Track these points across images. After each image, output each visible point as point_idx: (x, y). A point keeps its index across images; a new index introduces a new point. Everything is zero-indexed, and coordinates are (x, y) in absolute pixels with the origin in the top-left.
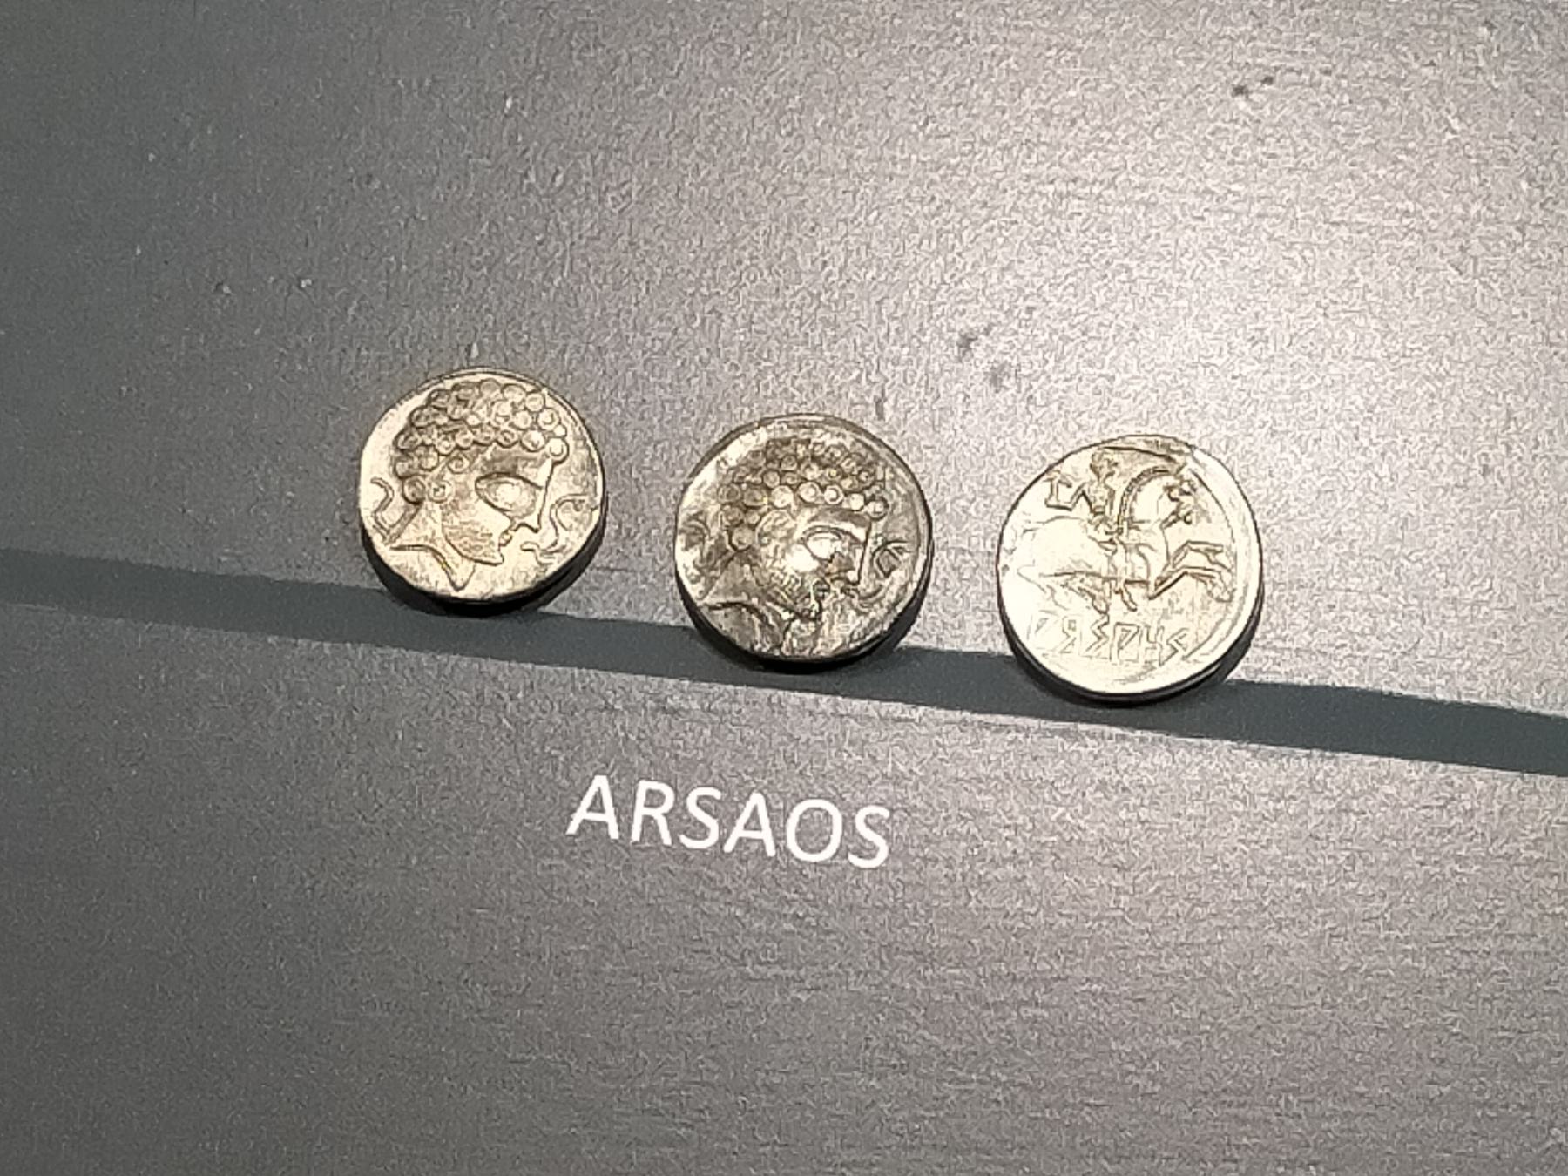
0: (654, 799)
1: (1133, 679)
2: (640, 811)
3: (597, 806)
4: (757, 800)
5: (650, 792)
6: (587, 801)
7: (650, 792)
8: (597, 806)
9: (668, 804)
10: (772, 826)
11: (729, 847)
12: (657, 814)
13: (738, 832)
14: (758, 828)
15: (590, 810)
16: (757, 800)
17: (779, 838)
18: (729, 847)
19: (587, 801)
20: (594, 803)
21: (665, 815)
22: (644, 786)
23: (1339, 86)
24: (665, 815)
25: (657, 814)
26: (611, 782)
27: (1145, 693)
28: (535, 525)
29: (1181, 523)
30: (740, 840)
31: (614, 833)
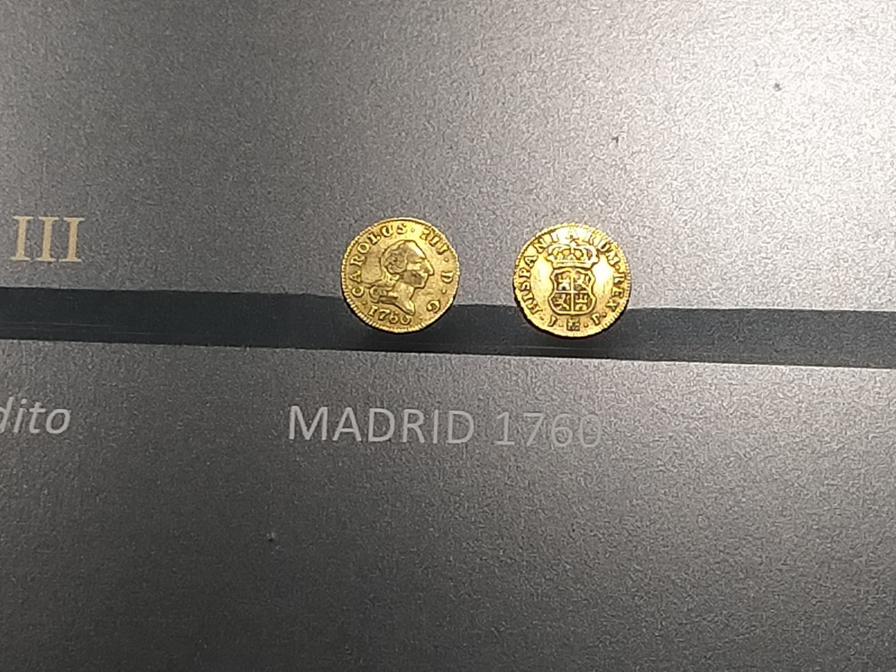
2: (406, 426)
3: (348, 424)
4: (349, 410)
6: (341, 424)
8: (348, 424)
9: (421, 422)
11: (335, 438)
12: (415, 426)
13: (340, 429)
14: (351, 427)
15: (344, 427)
18: (335, 438)
19: (341, 424)
20: (345, 423)
21: (420, 426)
23: (630, 634)
24: (420, 426)
25: (415, 426)
29: (532, 270)
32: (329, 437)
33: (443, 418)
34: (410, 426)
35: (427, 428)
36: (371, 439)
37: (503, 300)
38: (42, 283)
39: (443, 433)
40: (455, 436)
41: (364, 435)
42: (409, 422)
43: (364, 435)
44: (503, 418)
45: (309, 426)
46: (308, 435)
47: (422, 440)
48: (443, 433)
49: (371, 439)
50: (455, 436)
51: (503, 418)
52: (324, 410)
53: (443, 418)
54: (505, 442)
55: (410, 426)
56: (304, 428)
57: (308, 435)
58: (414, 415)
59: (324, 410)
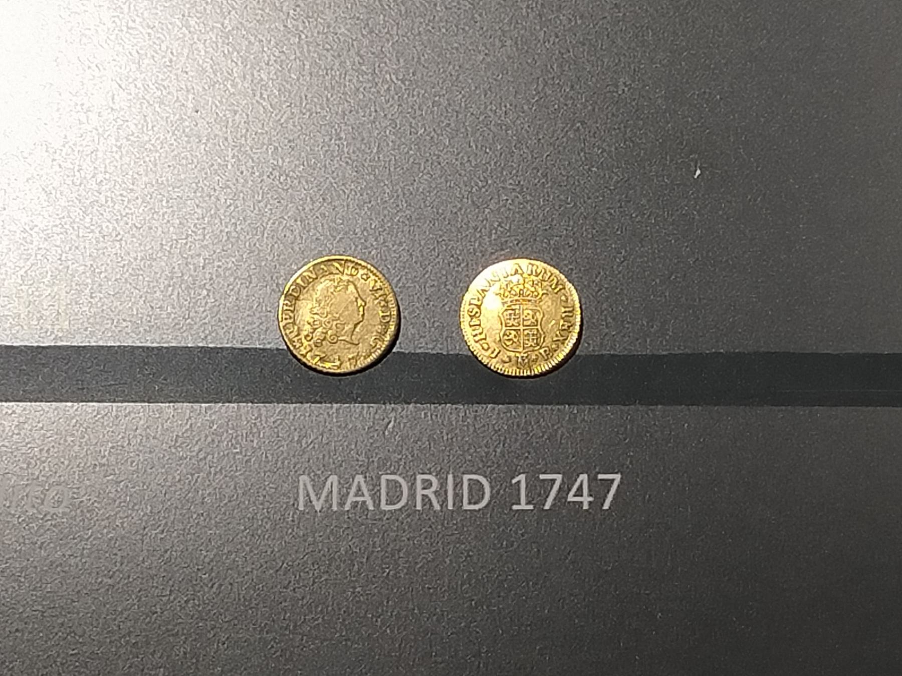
0: (427, 485)
2: (420, 492)
4: (359, 478)
7: (424, 481)
8: (579, 493)
13: (351, 499)
24: (435, 492)
32: (341, 504)
33: (458, 485)
34: (425, 492)
35: (441, 493)
36: (384, 507)
37: (272, 342)
38: (322, 360)
39: (458, 496)
40: (390, 502)
41: (377, 505)
43: (377, 505)
44: (519, 482)
47: (437, 507)
48: (458, 496)
49: (466, 507)
50: (390, 502)
51: (519, 482)
52: (333, 479)
53: (458, 485)
54: (523, 506)
55: (425, 492)
56: (313, 497)
58: (427, 480)
59: (333, 479)
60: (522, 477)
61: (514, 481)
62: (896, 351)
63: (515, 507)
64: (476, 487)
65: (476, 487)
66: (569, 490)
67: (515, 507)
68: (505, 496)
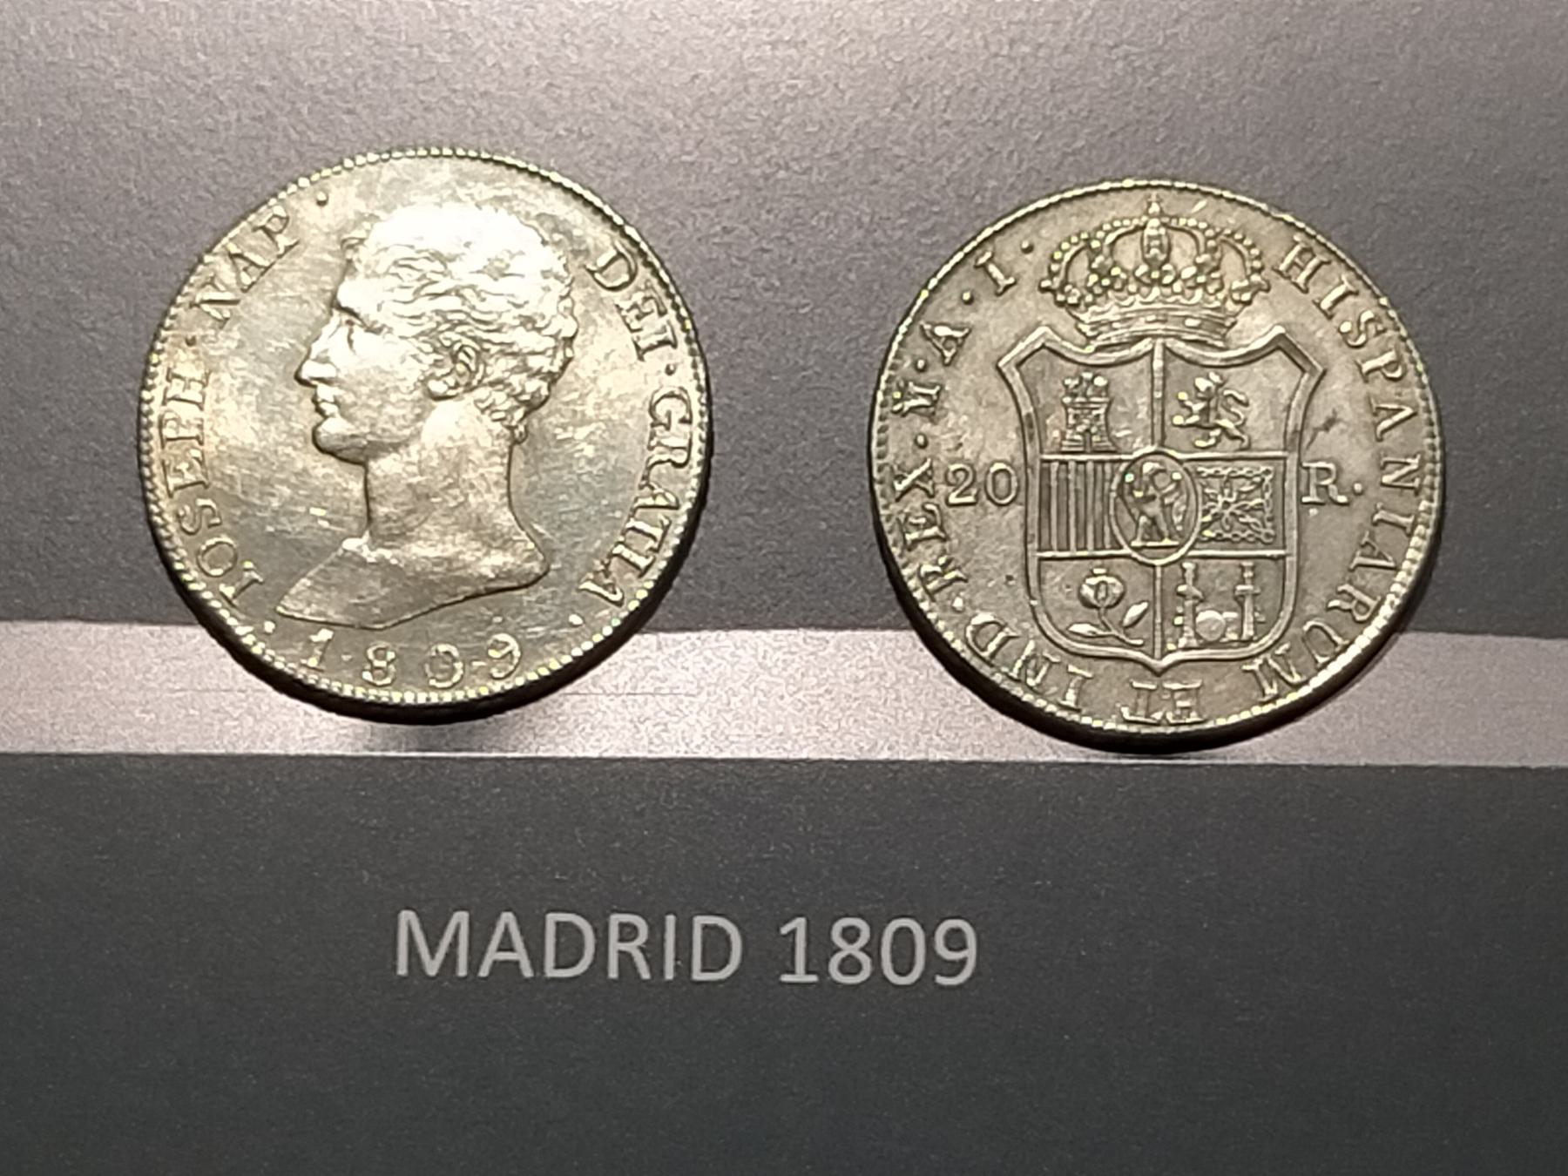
0: (628, 933)
1: (263, 691)
2: (615, 946)
3: (507, 945)
4: (507, 918)
5: (622, 926)
7: (622, 926)
8: (507, 945)
10: (527, 946)
11: (484, 972)
12: (631, 947)
13: (493, 955)
15: (500, 950)
16: (507, 918)
17: (537, 960)
18: (484, 972)
20: (502, 943)
22: (616, 919)
25: (631, 947)
26: (419, 915)
27: (1355, 659)
28: (199, 399)
30: (495, 962)
31: (528, 972)
32: (474, 966)
34: (625, 947)
35: (654, 952)
42: (622, 940)
44: (793, 932)
45: (433, 951)
46: (432, 967)
49: (698, 975)
51: (793, 932)
52: (461, 918)
54: (800, 976)
55: (625, 947)
57: (432, 967)
60: (799, 924)
61: (785, 930)
62: (1563, 763)
63: (786, 978)
64: (717, 940)
65: (717, 940)
66: (488, 941)
67: (786, 978)
68: (769, 954)
